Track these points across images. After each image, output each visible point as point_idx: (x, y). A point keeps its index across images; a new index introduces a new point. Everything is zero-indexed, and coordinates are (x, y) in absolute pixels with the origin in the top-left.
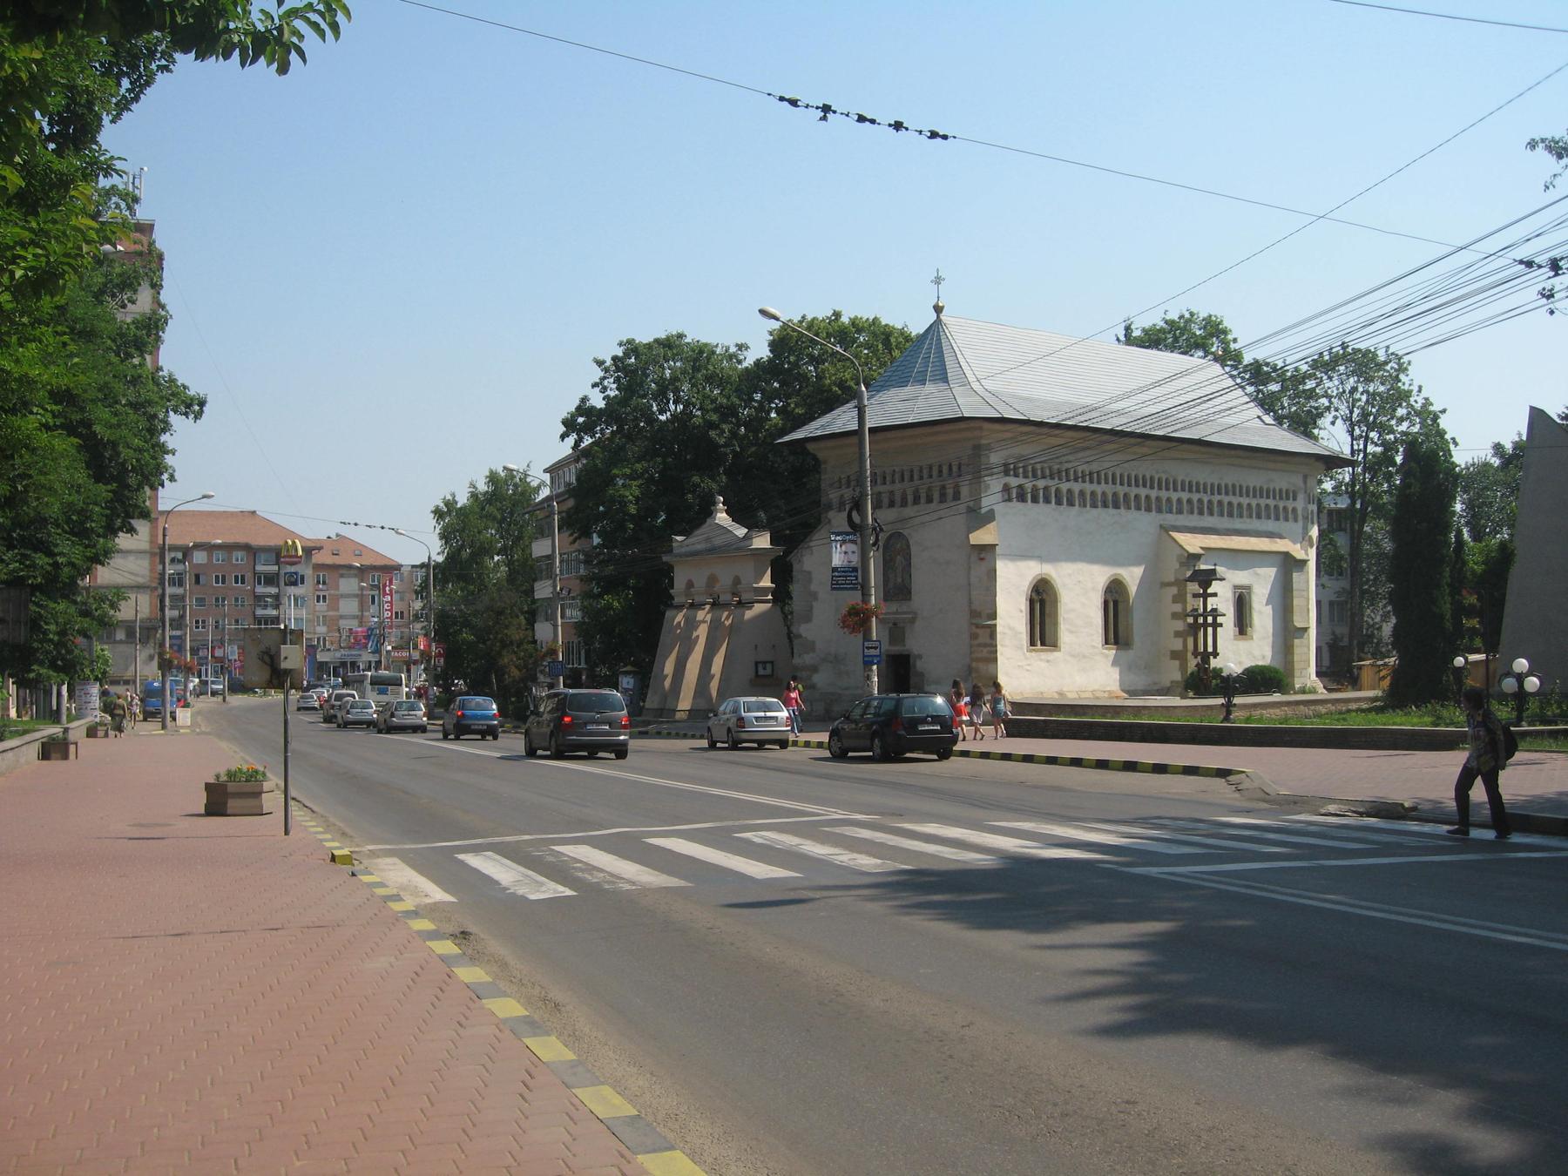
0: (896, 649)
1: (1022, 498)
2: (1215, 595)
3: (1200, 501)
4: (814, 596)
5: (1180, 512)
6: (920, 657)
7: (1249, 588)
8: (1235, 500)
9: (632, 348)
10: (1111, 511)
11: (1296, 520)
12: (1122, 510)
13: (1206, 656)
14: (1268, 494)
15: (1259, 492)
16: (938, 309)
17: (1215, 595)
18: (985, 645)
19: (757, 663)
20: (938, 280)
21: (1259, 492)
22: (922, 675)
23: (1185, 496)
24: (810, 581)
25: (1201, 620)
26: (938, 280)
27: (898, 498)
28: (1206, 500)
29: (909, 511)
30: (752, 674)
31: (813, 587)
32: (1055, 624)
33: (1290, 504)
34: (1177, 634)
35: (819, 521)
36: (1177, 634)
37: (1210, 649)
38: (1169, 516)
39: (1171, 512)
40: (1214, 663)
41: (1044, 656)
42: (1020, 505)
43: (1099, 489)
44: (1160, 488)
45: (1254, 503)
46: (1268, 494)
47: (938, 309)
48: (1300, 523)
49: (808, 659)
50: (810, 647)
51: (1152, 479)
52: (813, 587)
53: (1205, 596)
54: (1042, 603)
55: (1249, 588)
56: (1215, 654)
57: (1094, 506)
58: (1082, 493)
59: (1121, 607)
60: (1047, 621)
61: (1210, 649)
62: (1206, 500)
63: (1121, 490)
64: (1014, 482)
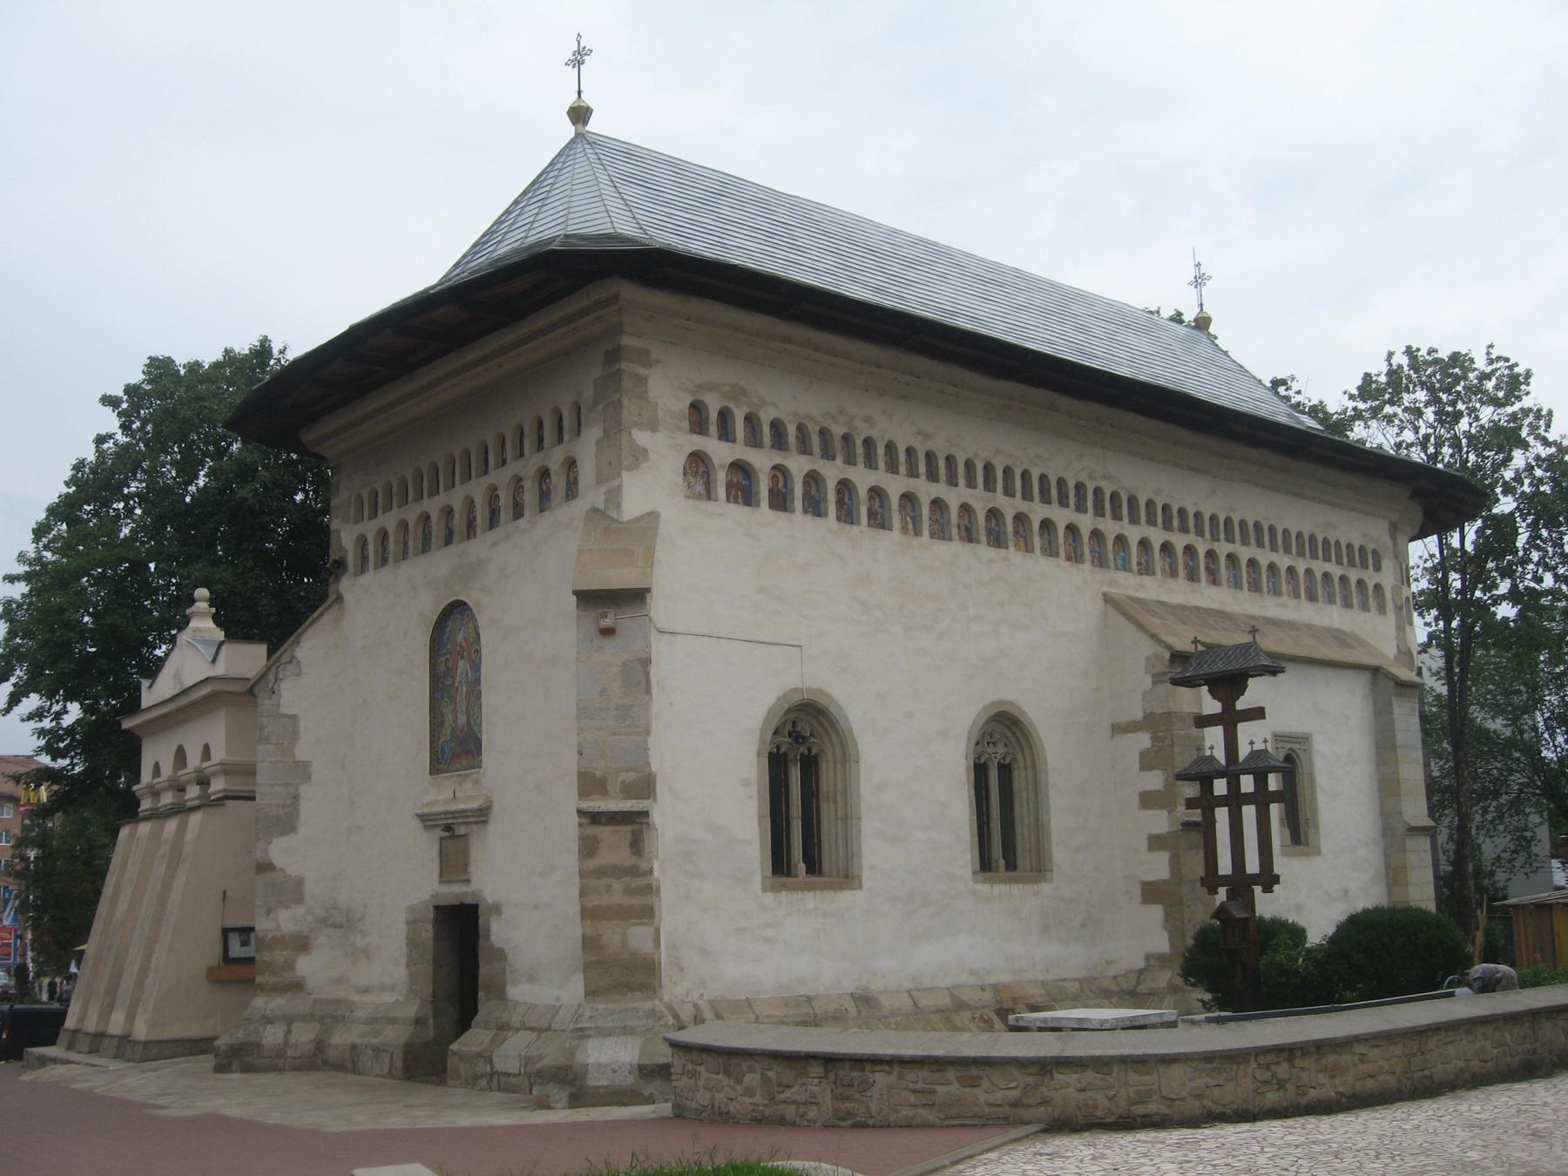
0: (453, 892)
1: (742, 486)
2: (1258, 713)
3: (1189, 550)
4: (303, 771)
5: (1146, 569)
6: (497, 908)
7: (1305, 739)
8: (1264, 557)
9: (160, 368)
10: (984, 551)
11: (1382, 610)
12: (1012, 553)
13: (1241, 886)
14: (1328, 550)
15: (1309, 546)
16: (579, 114)
17: (1258, 713)
18: (618, 872)
19: (226, 932)
20: (578, 59)
21: (1309, 546)
22: (500, 955)
23: (1157, 536)
24: (294, 736)
25: (1220, 787)
26: (578, 59)
27: (459, 519)
28: (1202, 550)
29: (479, 547)
30: (212, 955)
31: (302, 752)
32: (848, 819)
33: (1371, 579)
34: (1156, 842)
35: (323, 597)
36: (1156, 842)
37: (1252, 865)
38: (1121, 576)
39: (1126, 567)
40: (1266, 905)
41: (811, 900)
42: (737, 511)
43: (953, 497)
44: (1099, 511)
45: (1086, 522)
46: (1328, 550)
47: (579, 114)
48: (1391, 617)
49: (286, 920)
50: (294, 891)
51: (1080, 487)
52: (302, 752)
53: (1230, 720)
54: (810, 765)
55: (1305, 739)
56: (1269, 880)
57: (940, 533)
58: (909, 498)
59: (1019, 779)
60: (827, 810)
61: (1252, 865)
62: (1202, 550)
63: (1010, 506)
64: (721, 453)
